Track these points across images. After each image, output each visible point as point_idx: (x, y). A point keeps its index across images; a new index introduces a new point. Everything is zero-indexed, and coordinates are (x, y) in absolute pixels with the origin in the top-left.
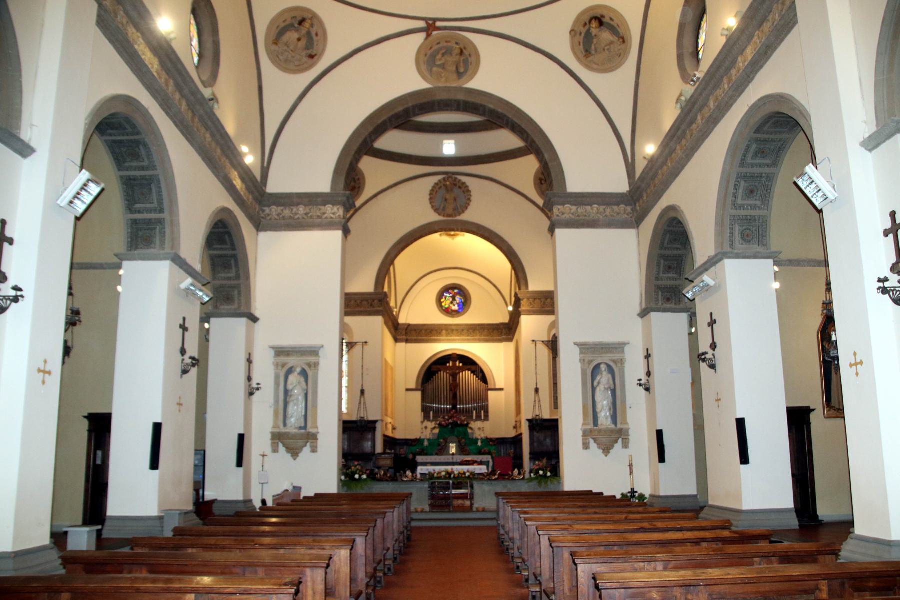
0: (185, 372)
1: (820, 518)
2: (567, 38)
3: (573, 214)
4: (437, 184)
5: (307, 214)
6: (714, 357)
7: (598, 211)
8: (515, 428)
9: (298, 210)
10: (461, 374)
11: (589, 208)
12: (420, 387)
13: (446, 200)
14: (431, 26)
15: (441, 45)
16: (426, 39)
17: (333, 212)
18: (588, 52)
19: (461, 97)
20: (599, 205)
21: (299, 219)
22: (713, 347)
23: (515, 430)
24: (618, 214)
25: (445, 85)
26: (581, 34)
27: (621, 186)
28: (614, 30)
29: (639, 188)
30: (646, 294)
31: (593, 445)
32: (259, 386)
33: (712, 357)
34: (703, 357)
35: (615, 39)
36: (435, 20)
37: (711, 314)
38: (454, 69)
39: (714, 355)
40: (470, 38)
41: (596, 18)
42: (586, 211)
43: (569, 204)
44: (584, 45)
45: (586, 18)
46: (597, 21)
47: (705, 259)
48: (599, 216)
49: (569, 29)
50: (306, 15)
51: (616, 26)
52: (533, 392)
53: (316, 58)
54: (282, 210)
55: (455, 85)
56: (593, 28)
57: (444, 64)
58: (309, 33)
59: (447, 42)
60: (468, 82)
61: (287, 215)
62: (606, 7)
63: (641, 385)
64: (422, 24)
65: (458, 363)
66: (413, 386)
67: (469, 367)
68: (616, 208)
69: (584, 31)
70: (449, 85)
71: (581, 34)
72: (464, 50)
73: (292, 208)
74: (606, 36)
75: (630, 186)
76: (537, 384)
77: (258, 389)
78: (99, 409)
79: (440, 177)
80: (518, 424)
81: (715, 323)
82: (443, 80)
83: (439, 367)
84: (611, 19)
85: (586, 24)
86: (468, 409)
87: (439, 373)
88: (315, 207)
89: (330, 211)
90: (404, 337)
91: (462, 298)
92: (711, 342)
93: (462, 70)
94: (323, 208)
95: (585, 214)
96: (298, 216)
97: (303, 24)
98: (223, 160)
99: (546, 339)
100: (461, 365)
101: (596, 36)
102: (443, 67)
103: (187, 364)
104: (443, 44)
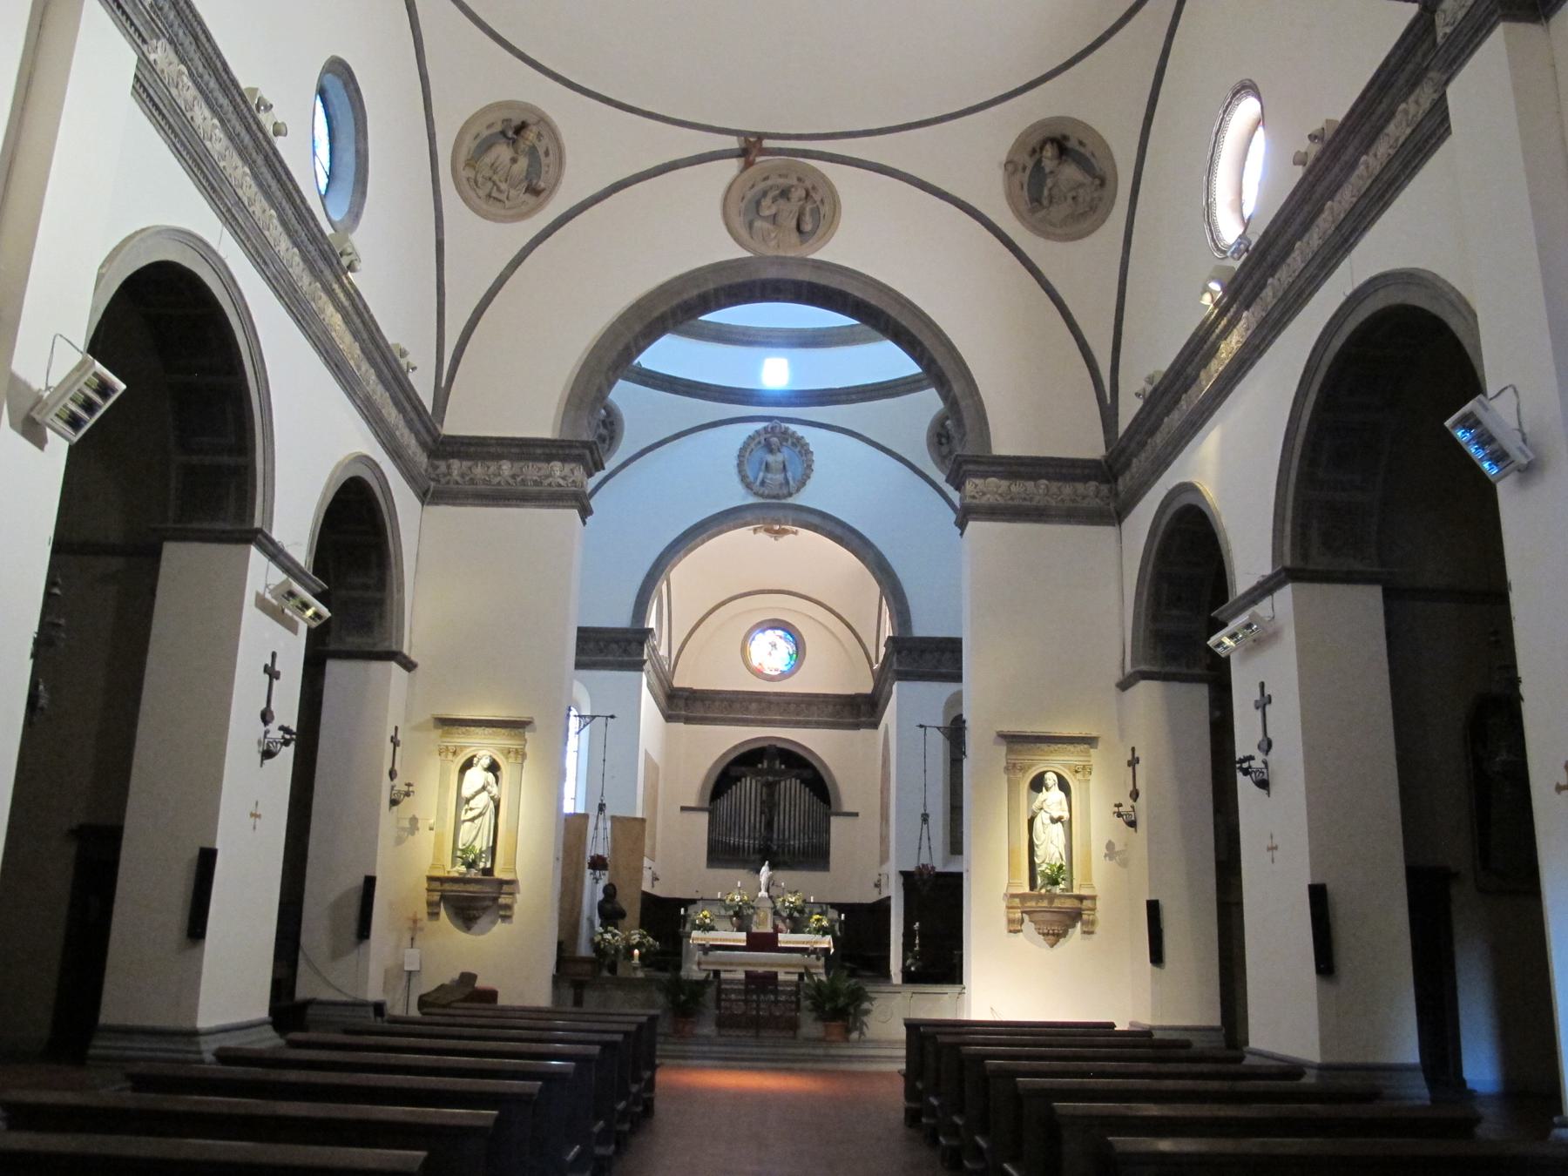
0: (268, 754)
1: (1469, 1086)
2: (998, 177)
3: (1001, 495)
4: (751, 438)
5: (514, 477)
6: (1267, 767)
7: (1048, 491)
8: (877, 885)
9: (500, 468)
10: (783, 784)
11: (1030, 484)
12: (706, 805)
13: (767, 465)
14: (750, 148)
15: (769, 183)
17: (563, 474)
18: (1036, 200)
19: (804, 276)
20: (1048, 478)
21: (499, 484)
22: (1265, 746)
23: (877, 890)
24: (1084, 498)
25: (775, 253)
27: (1091, 446)
28: (1084, 163)
29: (1123, 450)
30: (1133, 646)
31: (1029, 926)
32: (411, 789)
33: (1263, 766)
34: (1245, 765)
35: (1088, 180)
36: (761, 136)
37: (1262, 685)
38: (794, 223)
39: (1265, 763)
40: (824, 171)
41: (1053, 140)
42: (1026, 490)
43: (993, 476)
44: (1029, 190)
45: (1034, 141)
46: (1055, 145)
47: (1253, 582)
48: (1049, 499)
49: (1004, 158)
50: (531, 119)
51: (1088, 155)
52: (919, 820)
53: (543, 195)
54: (470, 468)
55: (791, 254)
57: (775, 216)
58: (533, 151)
61: (478, 476)
63: (1119, 815)
64: (733, 143)
65: (777, 762)
66: (692, 802)
67: (797, 771)
68: (1080, 487)
69: (1030, 164)
70: (782, 254)
71: (1024, 169)
73: (488, 463)
74: (1070, 172)
75: (1107, 448)
76: (925, 805)
77: (407, 794)
78: (370, 873)
79: (760, 426)
80: (883, 881)
81: (1270, 702)
82: (773, 243)
83: (743, 769)
84: (1081, 143)
85: (1034, 151)
86: (792, 848)
87: (743, 780)
88: (530, 464)
89: (558, 473)
90: (683, 713)
91: (789, 646)
92: (1131, 788)
93: (807, 227)
94: (544, 465)
95: (1023, 496)
96: (498, 479)
97: (522, 133)
98: (363, 369)
99: (941, 725)
100: (783, 767)
101: (1052, 172)
102: (774, 219)
103: (399, 791)
104: (776, 180)
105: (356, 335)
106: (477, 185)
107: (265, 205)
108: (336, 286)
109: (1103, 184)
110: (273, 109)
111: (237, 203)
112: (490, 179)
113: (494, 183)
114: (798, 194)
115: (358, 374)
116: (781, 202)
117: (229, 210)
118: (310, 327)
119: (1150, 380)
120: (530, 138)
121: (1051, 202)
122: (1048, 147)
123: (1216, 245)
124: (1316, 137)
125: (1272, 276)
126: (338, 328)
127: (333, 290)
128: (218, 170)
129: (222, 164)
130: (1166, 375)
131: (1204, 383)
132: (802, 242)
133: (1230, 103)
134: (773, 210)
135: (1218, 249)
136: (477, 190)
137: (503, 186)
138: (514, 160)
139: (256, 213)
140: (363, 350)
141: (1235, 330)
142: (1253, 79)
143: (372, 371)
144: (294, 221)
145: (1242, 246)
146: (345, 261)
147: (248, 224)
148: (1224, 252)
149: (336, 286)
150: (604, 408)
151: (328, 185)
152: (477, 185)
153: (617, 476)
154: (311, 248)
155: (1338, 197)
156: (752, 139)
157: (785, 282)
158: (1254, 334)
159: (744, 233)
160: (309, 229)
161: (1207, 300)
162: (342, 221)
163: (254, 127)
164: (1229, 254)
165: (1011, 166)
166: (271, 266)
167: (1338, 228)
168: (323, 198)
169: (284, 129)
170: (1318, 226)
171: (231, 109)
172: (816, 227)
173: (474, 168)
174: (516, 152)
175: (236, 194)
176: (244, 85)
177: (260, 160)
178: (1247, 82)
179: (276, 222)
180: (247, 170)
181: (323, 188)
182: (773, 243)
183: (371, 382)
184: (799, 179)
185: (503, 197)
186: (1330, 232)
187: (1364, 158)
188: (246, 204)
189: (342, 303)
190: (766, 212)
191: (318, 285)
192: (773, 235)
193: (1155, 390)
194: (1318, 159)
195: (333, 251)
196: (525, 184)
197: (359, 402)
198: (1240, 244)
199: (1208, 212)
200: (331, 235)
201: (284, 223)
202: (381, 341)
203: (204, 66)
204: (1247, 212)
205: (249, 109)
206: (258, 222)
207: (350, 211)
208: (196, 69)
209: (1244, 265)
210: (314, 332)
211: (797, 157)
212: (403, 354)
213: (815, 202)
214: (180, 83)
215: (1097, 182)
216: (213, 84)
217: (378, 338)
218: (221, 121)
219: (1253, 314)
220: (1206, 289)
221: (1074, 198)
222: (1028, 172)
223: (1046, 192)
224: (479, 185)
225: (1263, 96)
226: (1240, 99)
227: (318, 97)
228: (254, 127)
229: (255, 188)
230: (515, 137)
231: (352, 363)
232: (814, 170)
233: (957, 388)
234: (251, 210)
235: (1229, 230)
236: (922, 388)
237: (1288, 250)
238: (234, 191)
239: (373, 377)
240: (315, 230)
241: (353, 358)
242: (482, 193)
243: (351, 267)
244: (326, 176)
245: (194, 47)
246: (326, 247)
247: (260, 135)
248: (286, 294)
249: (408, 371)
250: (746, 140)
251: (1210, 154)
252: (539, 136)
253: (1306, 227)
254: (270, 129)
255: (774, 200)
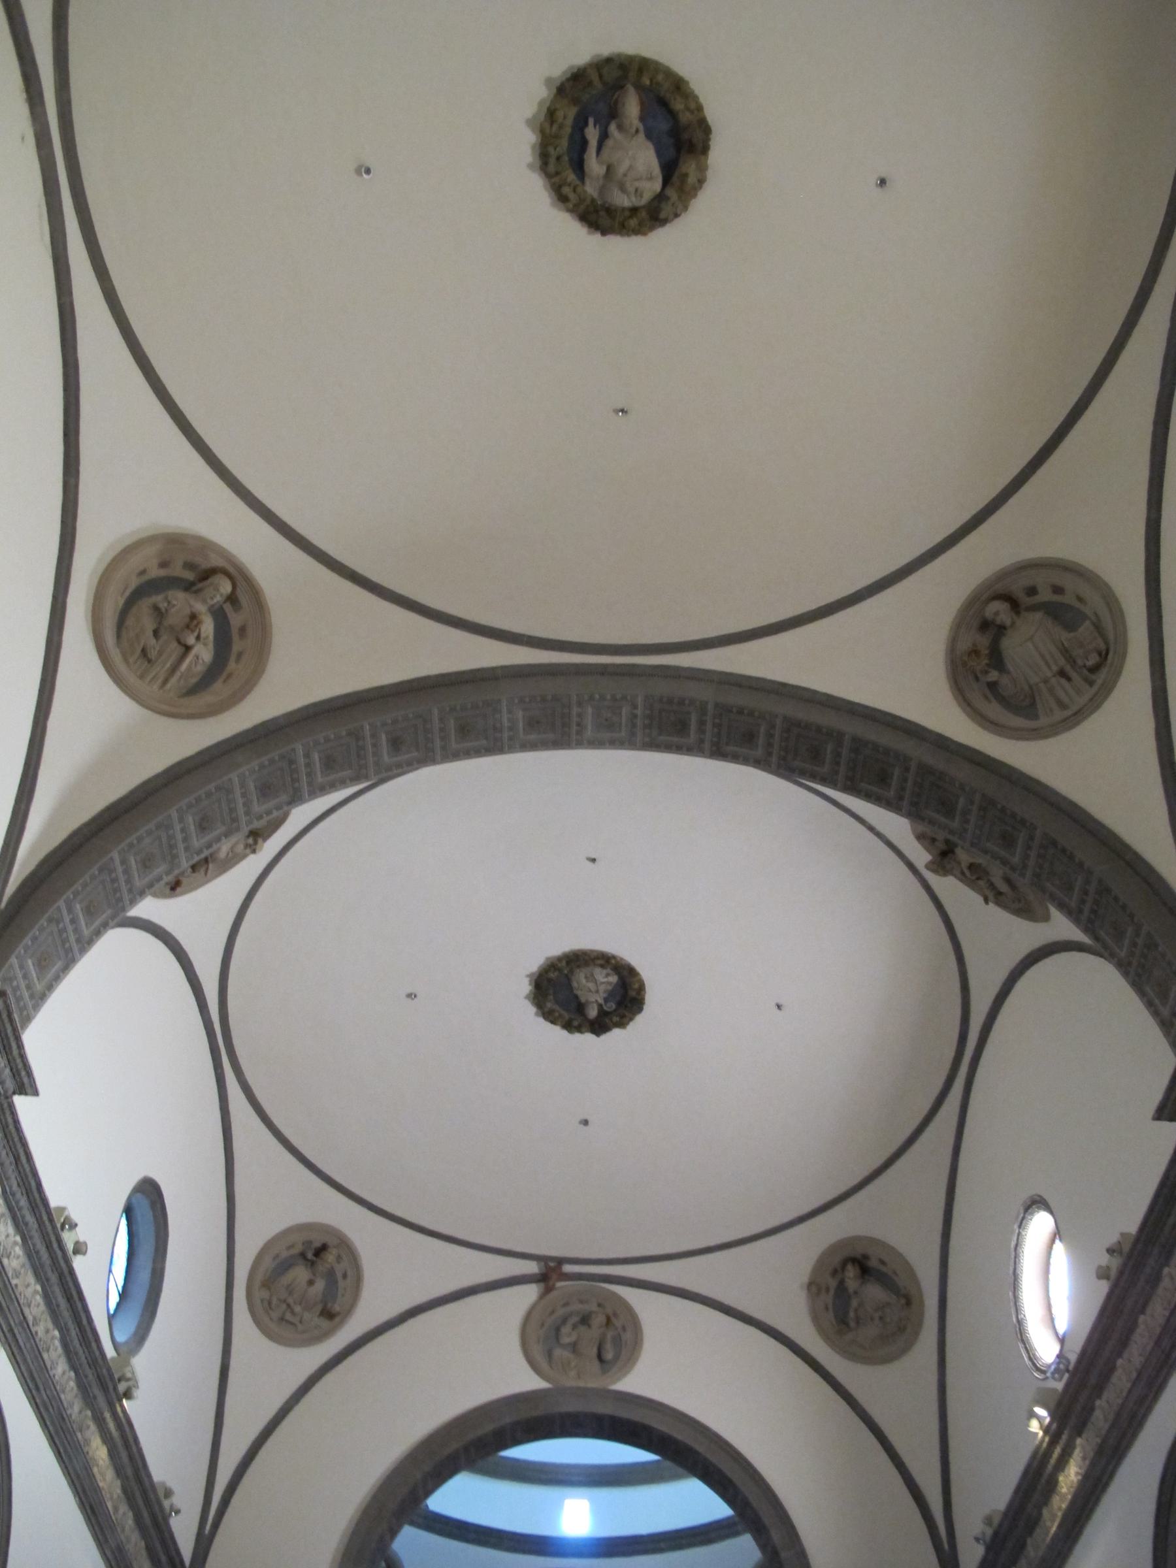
16: (542, 1296)
19: (605, 1408)
26: (828, 1290)
28: (886, 1281)
36: (561, 1261)
38: (595, 1350)
41: (854, 1260)
53: (337, 1319)
56: (849, 1278)
58: (331, 1276)
59: (581, 1302)
60: (619, 1379)
62: (873, 1241)
64: (532, 1268)
69: (833, 1283)
70: (581, 1384)
71: (828, 1290)
72: (614, 1320)
74: (874, 1293)
84: (883, 1262)
85: (835, 1273)
93: (609, 1355)
98: (121, 1511)
101: (856, 1293)
102: (574, 1347)
104: (576, 1307)
105: (119, 1471)
106: (270, 1308)
107: (50, 1326)
108: (107, 1415)
109: (908, 1303)
110: (77, 1229)
111: (21, 1324)
112: (285, 1301)
113: (289, 1306)
114: (598, 1320)
115: (113, 1518)
116: (582, 1329)
117: (11, 1330)
118: (32, 1347)
119: (988, 1521)
120: (329, 1260)
121: (858, 1323)
122: (850, 1267)
123: (1034, 1364)
124: (1114, 1251)
125: (1099, 1397)
126: (101, 1462)
127: (104, 1419)
128: (9, 1286)
129: (14, 1282)
130: (1006, 1514)
131: (1048, 1524)
132: (604, 1371)
133: (1023, 1218)
134: (573, 1338)
135: (1038, 1369)
136: (270, 1312)
137: (298, 1309)
138: (311, 1283)
139: (39, 1334)
140: (125, 1490)
141: (1072, 1460)
142: (1042, 1194)
143: (130, 1514)
144: (76, 1342)
145: (1062, 1366)
146: (122, 1387)
147: (28, 1346)
148: (1043, 1372)
149: (107, 1415)
150: (385, 1561)
151: (119, 1305)
152: (270, 1308)
153: (23, 110)
154: (89, 1372)
155: (1149, 1311)
156: (552, 1264)
157: (586, 1415)
158: (1093, 1465)
159: (544, 1365)
160: (91, 1352)
161: (1034, 1426)
162: (126, 1343)
163: (55, 1245)
164: (1049, 1374)
165: (814, 1287)
166: (43, 1392)
167: (1158, 1343)
168: (111, 1318)
169: (84, 1248)
170: (1136, 1343)
171: (36, 1226)
172: (617, 1357)
173: (269, 1289)
174: (314, 1275)
175: (23, 1314)
176: (54, 1201)
177: (54, 1278)
178: (1036, 1197)
179: (57, 1343)
180: (39, 1288)
181: (112, 1306)
182: (573, 1373)
183: (127, 1528)
184: (599, 1305)
185: (295, 1320)
186: (1149, 1348)
187: (1166, 1270)
188: (31, 1323)
189: (110, 1434)
190: (566, 1340)
191: (89, 1413)
192: (573, 1364)
193: (996, 1534)
194: (1121, 1273)
195: (111, 1376)
196: (319, 1308)
197: (109, 1553)
198: (1058, 1363)
199: (1020, 1329)
200: (113, 1359)
201: (65, 1345)
202: (146, 1479)
203: (18, 1185)
204: (1061, 1329)
205: (54, 1227)
206: (18, 1296)
207: (135, 1334)
208: (11, 1187)
209: (1067, 1385)
210: (75, 1470)
211: (595, 1281)
212: (168, 1493)
213: (616, 1329)
214: (13, 1253)
215: (903, 1301)
216: (23, 1202)
217: (143, 1475)
218: (24, 1239)
219: (1087, 1440)
220: (1033, 1415)
221: (881, 1318)
222: (832, 1292)
223: (852, 1314)
224: (273, 1306)
225: (1054, 1210)
226: (1032, 1214)
227: (124, 1215)
228: (55, 1245)
229: (43, 1307)
230: (314, 1258)
231: (109, 1505)
232: (614, 1294)
233: (776, 1536)
234: (33, 1330)
235: (1047, 1351)
236: (736, 1534)
237: (1110, 1369)
238: (22, 1311)
239: (130, 1522)
240: (97, 1353)
241: (111, 1498)
242: (275, 1315)
243: (128, 1395)
244: (113, 1271)
245: (13, 1167)
246: (104, 1371)
247: (59, 1253)
248: (53, 1423)
249: (170, 1515)
250: (546, 1264)
251: (1011, 1269)
252: (339, 1259)
253: (1124, 1343)
254: (70, 1247)
255: (574, 1327)
